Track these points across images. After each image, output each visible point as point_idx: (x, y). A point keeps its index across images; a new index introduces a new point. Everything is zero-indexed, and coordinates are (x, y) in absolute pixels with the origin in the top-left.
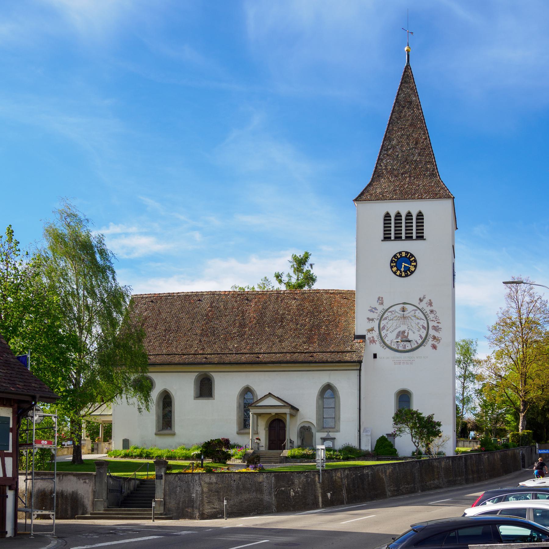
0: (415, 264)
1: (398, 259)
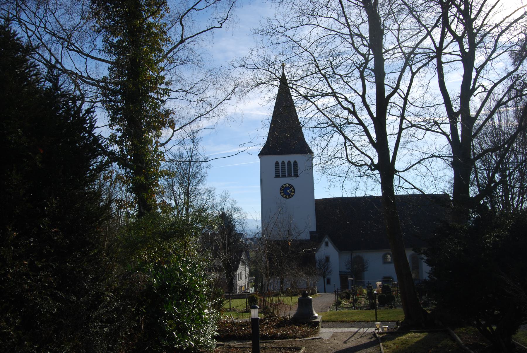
0: (294, 191)
1: (284, 188)
